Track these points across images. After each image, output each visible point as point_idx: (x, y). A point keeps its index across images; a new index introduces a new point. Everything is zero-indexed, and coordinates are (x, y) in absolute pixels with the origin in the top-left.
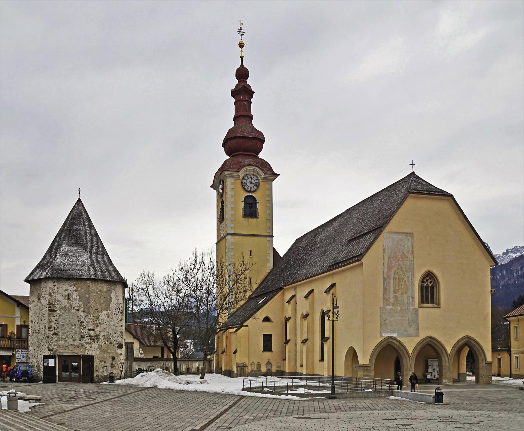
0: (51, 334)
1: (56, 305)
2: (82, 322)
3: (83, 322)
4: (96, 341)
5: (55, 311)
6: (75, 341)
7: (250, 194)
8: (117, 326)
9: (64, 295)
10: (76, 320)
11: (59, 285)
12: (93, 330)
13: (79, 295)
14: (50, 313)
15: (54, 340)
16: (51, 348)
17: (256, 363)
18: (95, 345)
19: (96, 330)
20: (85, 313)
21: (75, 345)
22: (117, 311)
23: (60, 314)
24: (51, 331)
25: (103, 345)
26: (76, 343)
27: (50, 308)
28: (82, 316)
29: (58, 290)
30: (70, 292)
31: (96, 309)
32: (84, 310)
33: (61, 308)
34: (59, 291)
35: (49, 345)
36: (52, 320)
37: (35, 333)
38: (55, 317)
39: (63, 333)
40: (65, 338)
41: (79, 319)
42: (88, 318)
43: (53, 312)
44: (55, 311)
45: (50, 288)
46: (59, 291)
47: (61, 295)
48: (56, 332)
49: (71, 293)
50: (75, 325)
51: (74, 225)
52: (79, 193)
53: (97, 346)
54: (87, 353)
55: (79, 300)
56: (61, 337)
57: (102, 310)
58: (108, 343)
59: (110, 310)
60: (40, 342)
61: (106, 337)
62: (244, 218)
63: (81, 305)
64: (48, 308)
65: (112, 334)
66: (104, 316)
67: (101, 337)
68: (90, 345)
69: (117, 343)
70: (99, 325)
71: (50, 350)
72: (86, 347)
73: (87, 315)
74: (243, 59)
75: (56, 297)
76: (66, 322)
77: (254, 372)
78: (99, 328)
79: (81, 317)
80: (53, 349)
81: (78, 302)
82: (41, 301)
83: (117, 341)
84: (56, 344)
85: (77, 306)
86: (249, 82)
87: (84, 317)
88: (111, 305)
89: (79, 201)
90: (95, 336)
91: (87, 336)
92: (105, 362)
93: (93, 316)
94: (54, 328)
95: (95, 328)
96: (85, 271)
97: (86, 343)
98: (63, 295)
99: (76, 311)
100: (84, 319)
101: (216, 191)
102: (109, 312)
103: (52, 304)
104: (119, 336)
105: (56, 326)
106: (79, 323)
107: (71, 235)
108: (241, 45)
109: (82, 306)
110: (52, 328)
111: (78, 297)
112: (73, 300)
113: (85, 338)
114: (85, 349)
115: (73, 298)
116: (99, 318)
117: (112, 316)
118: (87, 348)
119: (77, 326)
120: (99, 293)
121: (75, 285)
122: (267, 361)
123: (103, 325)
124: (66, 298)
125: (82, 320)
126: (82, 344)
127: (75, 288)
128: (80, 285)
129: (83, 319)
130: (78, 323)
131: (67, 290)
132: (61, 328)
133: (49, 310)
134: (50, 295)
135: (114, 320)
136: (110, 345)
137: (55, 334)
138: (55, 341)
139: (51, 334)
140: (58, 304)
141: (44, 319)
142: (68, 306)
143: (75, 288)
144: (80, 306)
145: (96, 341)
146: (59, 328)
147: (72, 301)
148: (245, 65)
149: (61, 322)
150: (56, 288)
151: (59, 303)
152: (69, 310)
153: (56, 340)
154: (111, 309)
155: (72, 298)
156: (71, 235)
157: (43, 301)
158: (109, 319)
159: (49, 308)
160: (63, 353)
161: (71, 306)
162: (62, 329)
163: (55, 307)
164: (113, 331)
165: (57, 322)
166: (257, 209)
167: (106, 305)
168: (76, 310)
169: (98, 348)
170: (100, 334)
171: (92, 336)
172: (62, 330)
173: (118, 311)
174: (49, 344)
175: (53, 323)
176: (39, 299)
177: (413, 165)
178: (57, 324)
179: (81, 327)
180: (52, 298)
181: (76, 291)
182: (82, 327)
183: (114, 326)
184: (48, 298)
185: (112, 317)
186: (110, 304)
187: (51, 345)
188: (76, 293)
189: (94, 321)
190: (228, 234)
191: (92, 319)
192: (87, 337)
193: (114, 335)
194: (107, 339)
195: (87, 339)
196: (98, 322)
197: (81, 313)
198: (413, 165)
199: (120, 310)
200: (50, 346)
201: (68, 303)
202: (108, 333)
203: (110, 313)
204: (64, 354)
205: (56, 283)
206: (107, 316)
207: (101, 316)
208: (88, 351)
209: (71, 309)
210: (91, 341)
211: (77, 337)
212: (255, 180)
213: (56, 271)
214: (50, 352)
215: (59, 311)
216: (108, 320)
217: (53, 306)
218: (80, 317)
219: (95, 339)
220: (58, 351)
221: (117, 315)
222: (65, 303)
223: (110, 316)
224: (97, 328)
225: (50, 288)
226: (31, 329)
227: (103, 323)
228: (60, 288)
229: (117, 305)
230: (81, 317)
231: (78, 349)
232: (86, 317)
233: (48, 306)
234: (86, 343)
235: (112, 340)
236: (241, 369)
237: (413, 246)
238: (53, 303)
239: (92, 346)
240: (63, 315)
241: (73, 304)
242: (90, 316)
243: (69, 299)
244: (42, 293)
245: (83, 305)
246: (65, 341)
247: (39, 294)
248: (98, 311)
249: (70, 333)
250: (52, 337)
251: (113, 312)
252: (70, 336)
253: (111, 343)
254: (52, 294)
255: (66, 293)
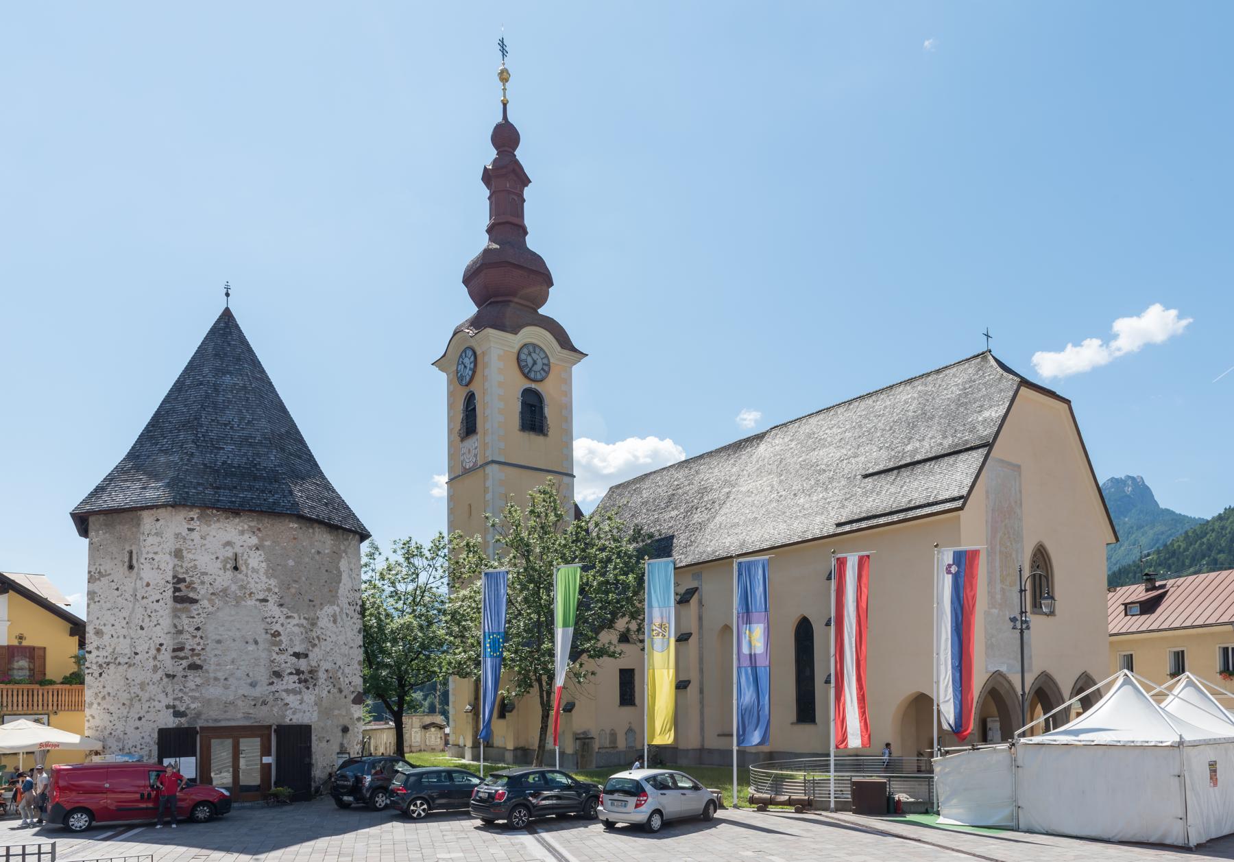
0: (183, 666)
1: (195, 586)
2: (276, 634)
3: (279, 634)
4: (311, 686)
5: (195, 601)
6: (254, 686)
7: (533, 386)
8: (352, 647)
9: (221, 557)
10: (260, 628)
11: (205, 528)
12: (306, 656)
13: (267, 560)
14: (179, 606)
15: (191, 685)
16: (182, 709)
17: (608, 732)
18: (309, 697)
19: (311, 655)
20: (285, 610)
21: (255, 699)
22: (352, 607)
23: (211, 609)
24: (182, 658)
25: (324, 696)
26: (257, 692)
27: (177, 594)
28: (277, 616)
29: (204, 542)
30: (239, 550)
31: (310, 601)
32: (282, 601)
33: (212, 594)
34: (207, 547)
35: (175, 699)
36: (186, 627)
37: (112, 667)
38: (193, 617)
39: (218, 665)
40: (226, 679)
41: (268, 627)
42: (292, 624)
43: (187, 605)
44: (195, 601)
45: (177, 535)
46: (207, 547)
47: (214, 557)
48: (198, 662)
49: (243, 554)
50: (256, 642)
51: (224, 374)
52: (227, 295)
53: (313, 698)
54: (291, 720)
55: (266, 573)
56: (212, 675)
57: (321, 604)
58: (336, 691)
59: (338, 605)
60: (136, 690)
61: (330, 675)
62: (521, 434)
63: (272, 587)
64: (169, 593)
65: (342, 667)
66: (326, 619)
67: (322, 675)
68: (299, 697)
69: (352, 689)
70: (317, 642)
71: (177, 714)
72: (286, 701)
73: (289, 614)
74: (508, 106)
75: (196, 563)
76: (229, 633)
77: (604, 751)
78: (316, 650)
79: (274, 620)
80: (188, 712)
81: (264, 579)
82: (138, 574)
83: (353, 684)
84: (197, 694)
85: (260, 588)
86: (519, 153)
87: (282, 620)
88: (339, 591)
89: (227, 316)
90: (311, 672)
91: (289, 671)
92: (328, 741)
93: (304, 618)
94: (193, 650)
95: (308, 650)
96: (285, 496)
97: (287, 691)
98: (217, 558)
99: (258, 603)
100: (282, 625)
101: (445, 374)
102: (336, 608)
103: (184, 580)
104: (356, 672)
105: (199, 644)
106: (269, 636)
107: (221, 399)
108: (504, 76)
109: (277, 590)
110: (186, 651)
111: (264, 565)
112: (249, 572)
113: (286, 678)
114: (284, 708)
115: (250, 566)
116: (316, 624)
117: (342, 619)
118: (291, 705)
119: (262, 646)
120: (317, 557)
121: (254, 532)
122: (627, 727)
123: (324, 643)
124: (228, 566)
125: (277, 627)
126: (277, 694)
127: (254, 540)
128: (269, 533)
129: (278, 625)
130: (264, 636)
131: (228, 544)
132: (213, 649)
133: (177, 600)
134: (178, 554)
135: (347, 630)
136: (338, 695)
137: (194, 667)
138: (194, 687)
139: (180, 668)
140: (203, 583)
141: (152, 624)
142: (234, 588)
143: (254, 540)
144: (269, 590)
145: (311, 686)
146: (208, 649)
147: (247, 576)
148: (510, 120)
149: (212, 631)
150: (195, 535)
151: (206, 579)
152: (238, 600)
153: (197, 685)
154: (339, 602)
155: (247, 567)
156: (221, 399)
157: (147, 573)
158: (337, 627)
159: (174, 592)
160: (220, 721)
161: (242, 587)
162: (217, 652)
163: (194, 589)
164: (345, 659)
165: (199, 633)
166: (545, 417)
167: (330, 591)
168: (257, 600)
169: (316, 704)
170: (319, 666)
171: (303, 672)
172: (216, 655)
173: (353, 608)
174: (175, 696)
175: (188, 636)
176: (131, 567)
177: (988, 336)
178: (201, 637)
179: (274, 648)
180: (184, 565)
181: (257, 549)
182: (277, 649)
183: (347, 647)
184: (171, 566)
185: (341, 623)
186: (339, 588)
187: (181, 699)
188: (258, 553)
189: (306, 633)
190: (493, 462)
191: (302, 625)
192: (291, 674)
193: (347, 670)
194: (333, 679)
195: (290, 682)
196: (314, 635)
197: (273, 609)
198: (988, 336)
199: (357, 604)
200: (177, 703)
201: (234, 581)
202: (335, 664)
203: (337, 613)
204: (223, 724)
205: (198, 523)
206: (332, 619)
207: (320, 619)
208: (294, 713)
209: (243, 598)
210: (301, 686)
211: (262, 675)
212: (542, 359)
213: (195, 488)
214: (177, 720)
215: (205, 603)
216: (335, 629)
217: (187, 587)
218: (269, 620)
219: (310, 680)
220: (203, 717)
221: (351, 618)
222: (224, 579)
223: (339, 620)
224: (314, 650)
225: (177, 535)
226: (95, 653)
227: (324, 638)
228: (209, 538)
229: (351, 592)
230: (274, 620)
231: (263, 707)
232: (288, 621)
233: (170, 586)
234: (287, 691)
235: (342, 683)
236: (584, 743)
237: (1020, 492)
238: (188, 580)
239: (302, 698)
240: (220, 614)
241: (248, 583)
242: (300, 618)
243: (236, 568)
244: (144, 551)
245: (280, 588)
246: (226, 688)
247: (131, 553)
248: (314, 606)
249: (242, 663)
250: (186, 676)
251: (344, 611)
252: (239, 673)
253: (341, 691)
254: (185, 553)
255: (229, 553)
